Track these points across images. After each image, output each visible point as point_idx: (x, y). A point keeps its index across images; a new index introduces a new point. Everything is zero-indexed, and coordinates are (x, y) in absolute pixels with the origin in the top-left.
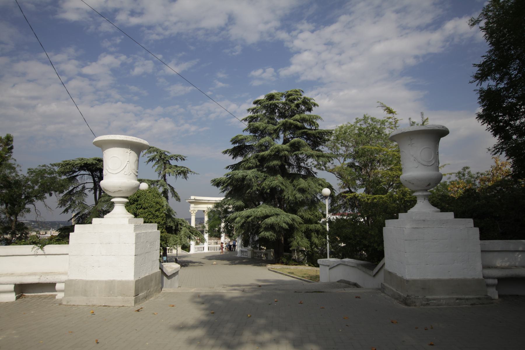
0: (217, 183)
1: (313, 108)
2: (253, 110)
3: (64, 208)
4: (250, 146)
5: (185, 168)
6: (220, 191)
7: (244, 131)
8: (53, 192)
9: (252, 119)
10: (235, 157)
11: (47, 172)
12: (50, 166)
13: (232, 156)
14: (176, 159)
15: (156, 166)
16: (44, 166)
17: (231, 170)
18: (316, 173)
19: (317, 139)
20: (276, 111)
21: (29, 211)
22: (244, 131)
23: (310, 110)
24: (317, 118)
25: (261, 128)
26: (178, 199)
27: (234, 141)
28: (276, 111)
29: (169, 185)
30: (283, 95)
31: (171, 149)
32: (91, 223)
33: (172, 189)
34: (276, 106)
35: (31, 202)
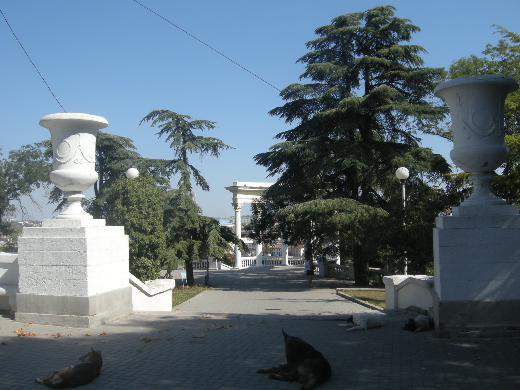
0: (263, 159)
1: (412, 34)
2: (314, 43)
3: (56, 205)
4: (310, 100)
5: (214, 139)
6: (269, 173)
7: (301, 77)
8: (40, 182)
9: (311, 58)
10: (289, 119)
11: (32, 155)
12: (34, 146)
13: (285, 118)
14: (200, 127)
15: (172, 140)
16: (28, 146)
17: (284, 140)
18: (419, 140)
19: (421, 81)
20: (354, 42)
21: (13, 209)
22: (301, 77)
23: (407, 37)
24: (416, 49)
25: (328, 71)
26: (206, 187)
27: (287, 93)
28: (354, 42)
29: (191, 166)
30: (361, 16)
31: (191, 112)
32: (125, 234)
33: (196, 173)
34: (352, 34)
35: (16, 196)
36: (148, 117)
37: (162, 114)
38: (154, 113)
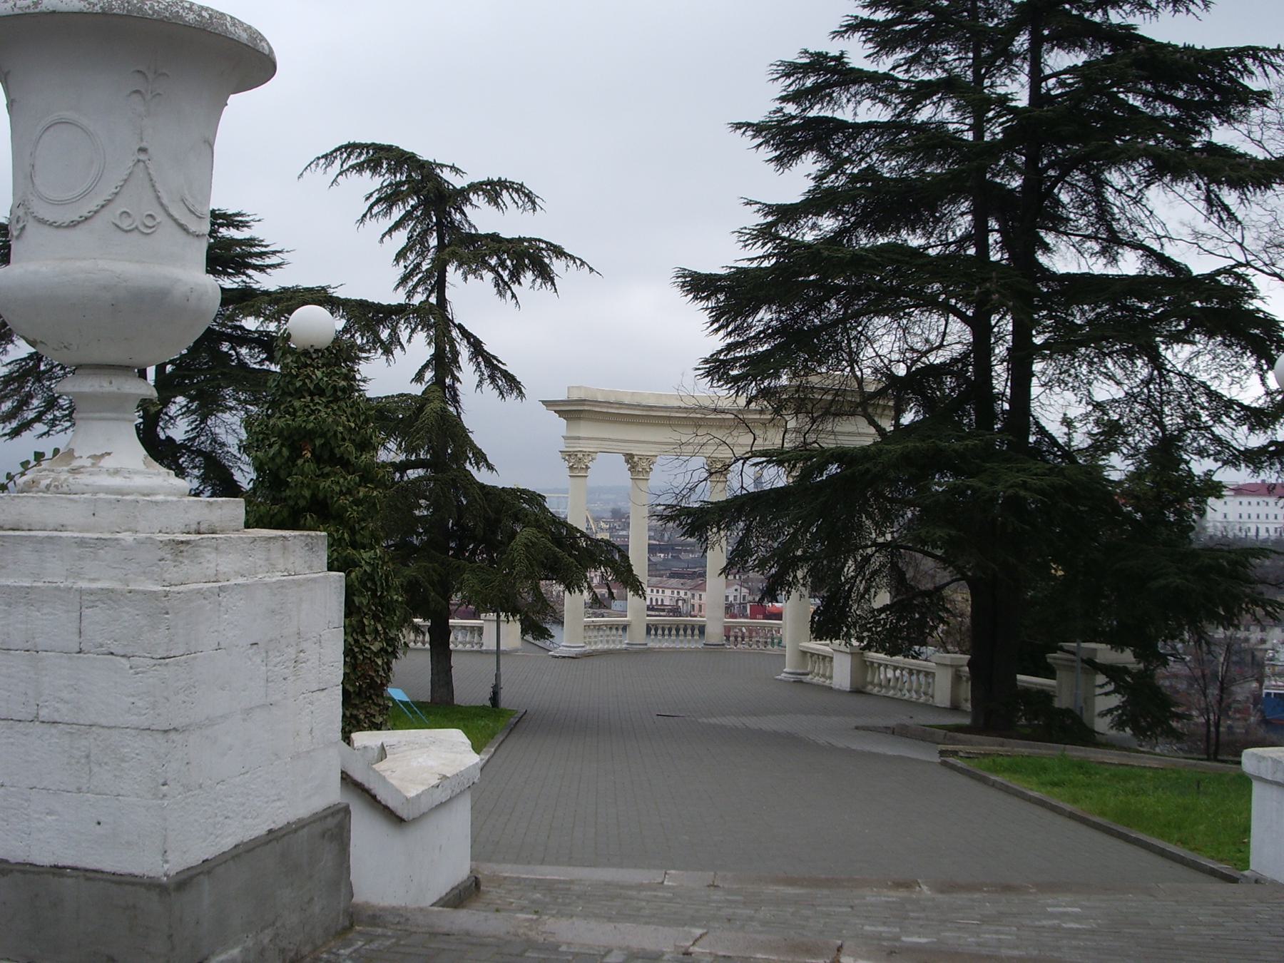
15: (401, 238)
29: (460, 327)
33: (477, 347)
36: (329, 157)
37: (379, 156)
38: (351, 148)
